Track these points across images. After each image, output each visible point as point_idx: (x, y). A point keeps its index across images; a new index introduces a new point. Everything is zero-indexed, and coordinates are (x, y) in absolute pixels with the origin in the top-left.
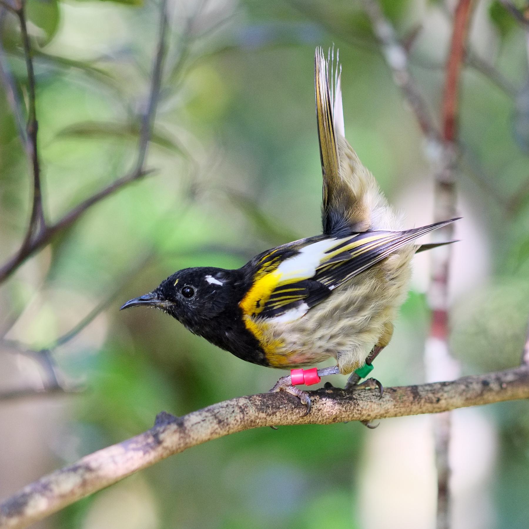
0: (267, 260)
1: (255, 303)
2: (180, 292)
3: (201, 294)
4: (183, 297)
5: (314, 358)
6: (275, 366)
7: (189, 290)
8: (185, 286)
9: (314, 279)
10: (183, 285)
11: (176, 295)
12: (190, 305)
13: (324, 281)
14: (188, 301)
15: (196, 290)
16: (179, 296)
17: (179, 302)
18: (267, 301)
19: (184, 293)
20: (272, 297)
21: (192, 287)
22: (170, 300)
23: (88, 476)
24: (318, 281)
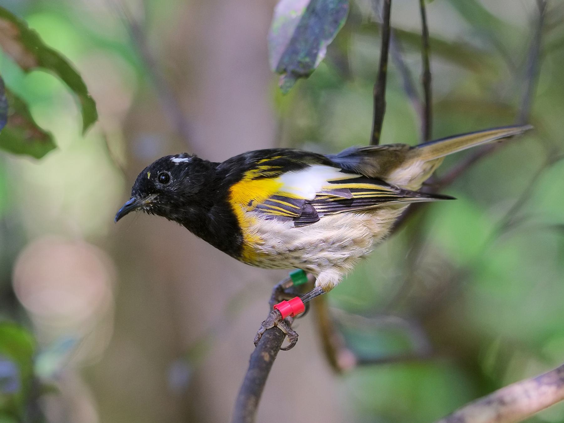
0: (276, 155)
1: (249, 201)
2: (157, 181)
3: (176, 176)
4: (162, 185)
5: (267, 219)
6: (294, 266)
7: (163, 177)
8: (159, 174)
9: (310, 203)
10: (157, 174)
11: (155, 186)
12: (171, 188)
13: (318, 208)
14: (169, 186)
15: (169, 173)
16: (159, 185)
17: (161, 190)
18: (260, 204)
19: (161, 181)
20: (267, 201)
21: (165, 172)
22: (152, 193)
23: (503, 410)
24: (312, 205)
